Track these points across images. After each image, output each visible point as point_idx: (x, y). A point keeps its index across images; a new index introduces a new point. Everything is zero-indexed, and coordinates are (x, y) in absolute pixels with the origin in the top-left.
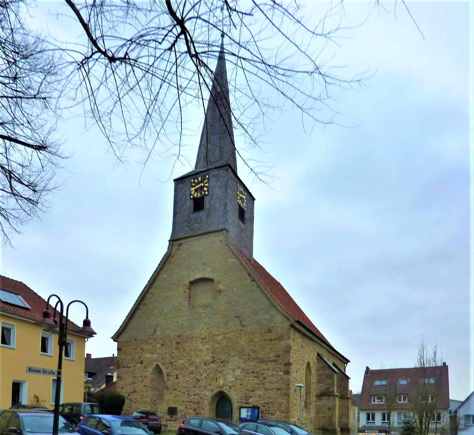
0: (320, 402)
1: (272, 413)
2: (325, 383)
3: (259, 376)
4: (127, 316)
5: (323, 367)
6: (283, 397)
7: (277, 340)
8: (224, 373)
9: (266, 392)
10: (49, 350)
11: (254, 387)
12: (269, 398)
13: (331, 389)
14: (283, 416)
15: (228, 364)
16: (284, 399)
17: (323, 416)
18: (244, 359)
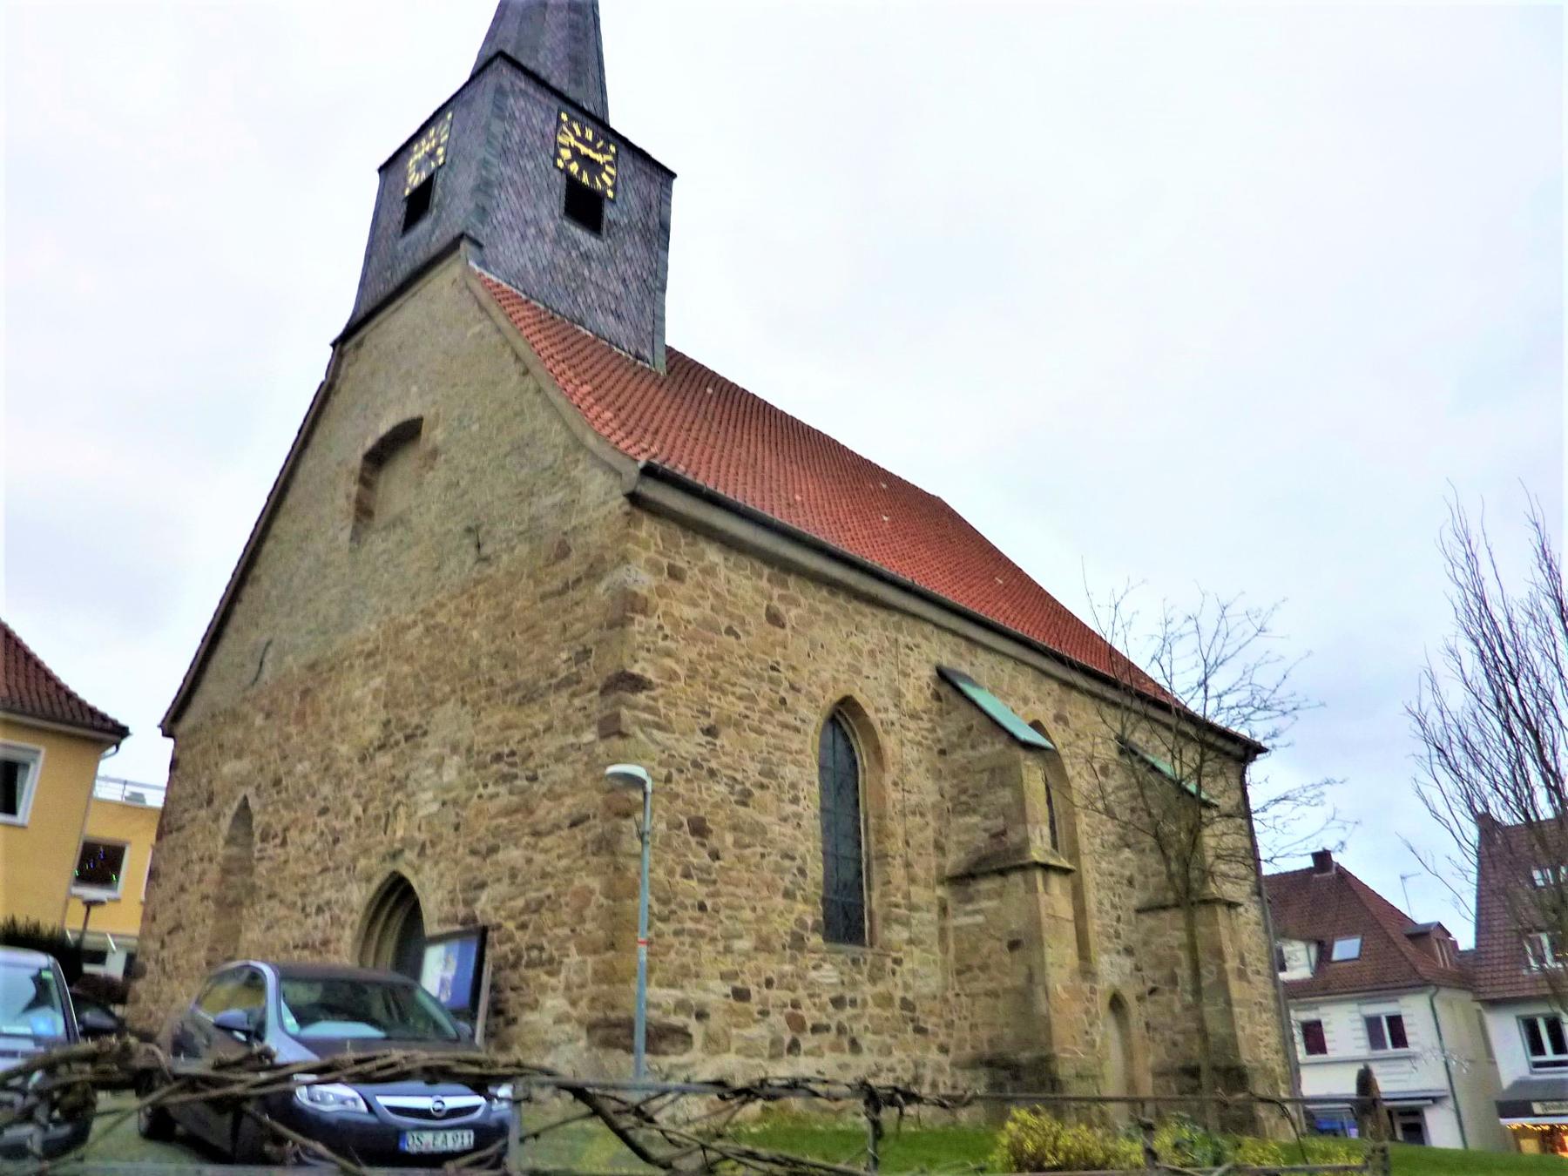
0: (967, 914)
1: (551, 960)
2: (983, 809)
3: (514, 770)
4: (206, 635)
5: (970, 728)
6: (594, 860)
7: (584, 582)
8: (411, 785)
9: (534, 847)
10: (21, 810)
11: (495, 832)
12: (544, 875)
13: (1013, 837)
14: (589, 972)
15: (426, 740)
16: (596, 872)
17: (991, 986)
18: (474, 704)
